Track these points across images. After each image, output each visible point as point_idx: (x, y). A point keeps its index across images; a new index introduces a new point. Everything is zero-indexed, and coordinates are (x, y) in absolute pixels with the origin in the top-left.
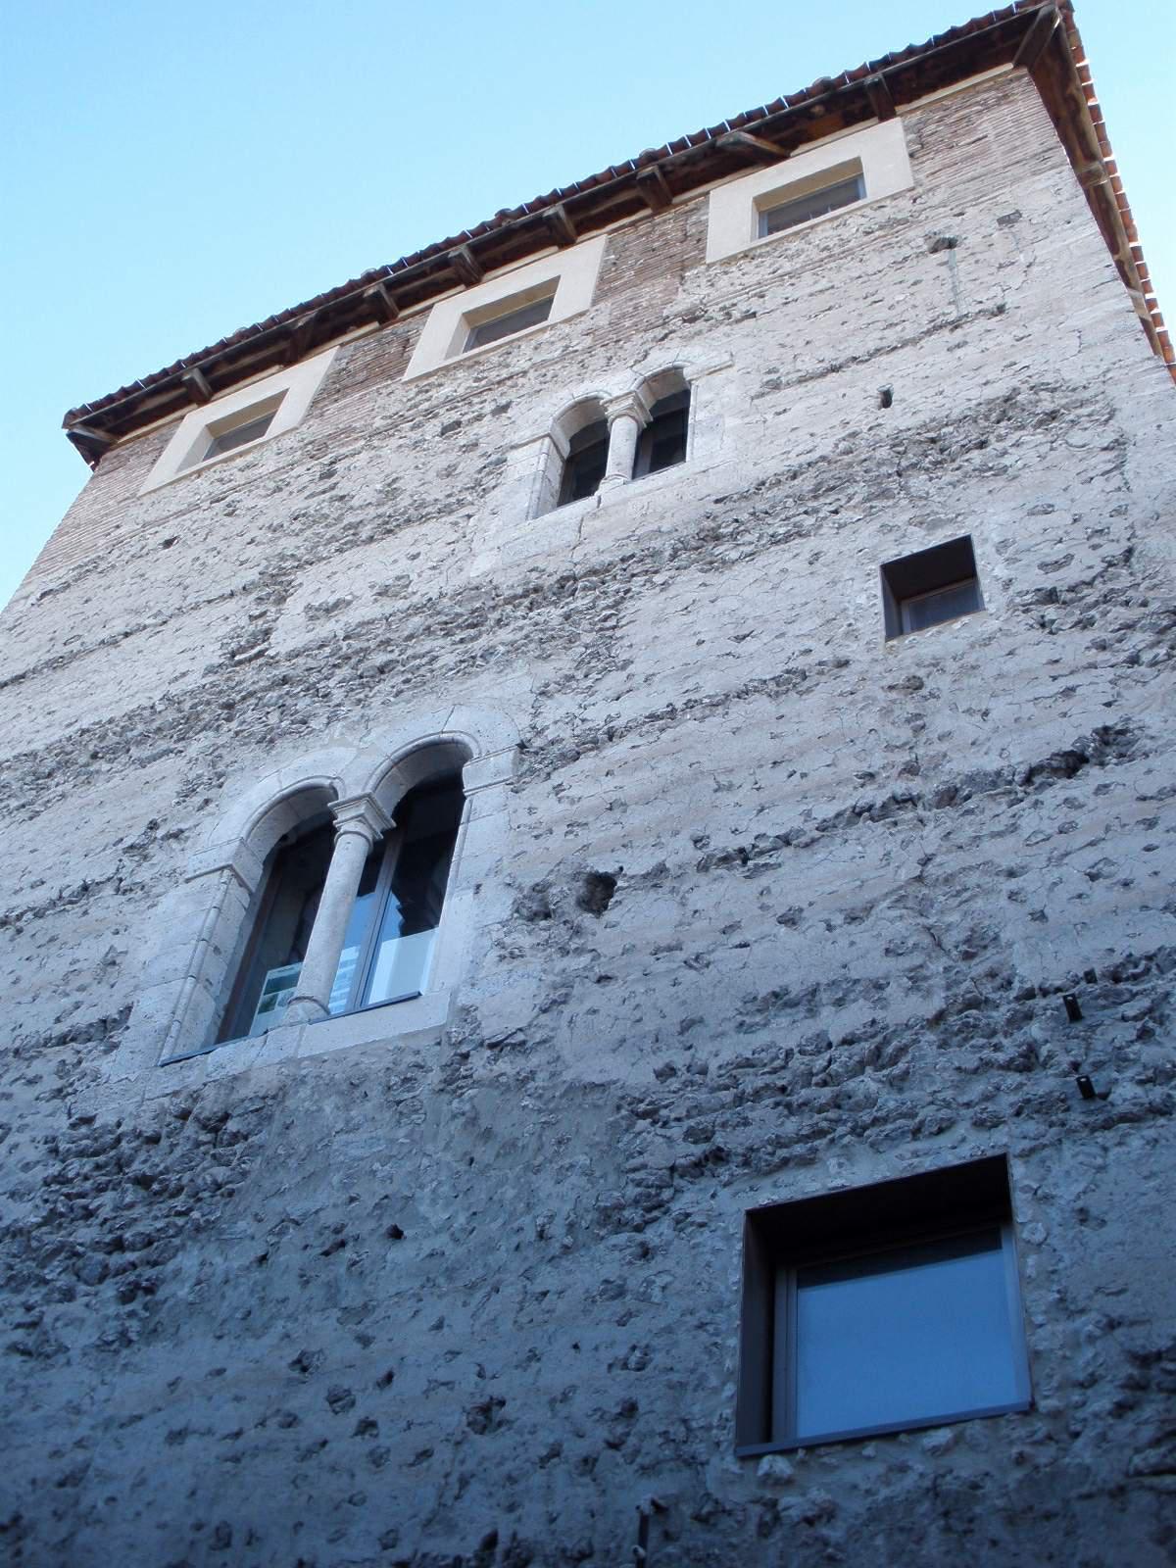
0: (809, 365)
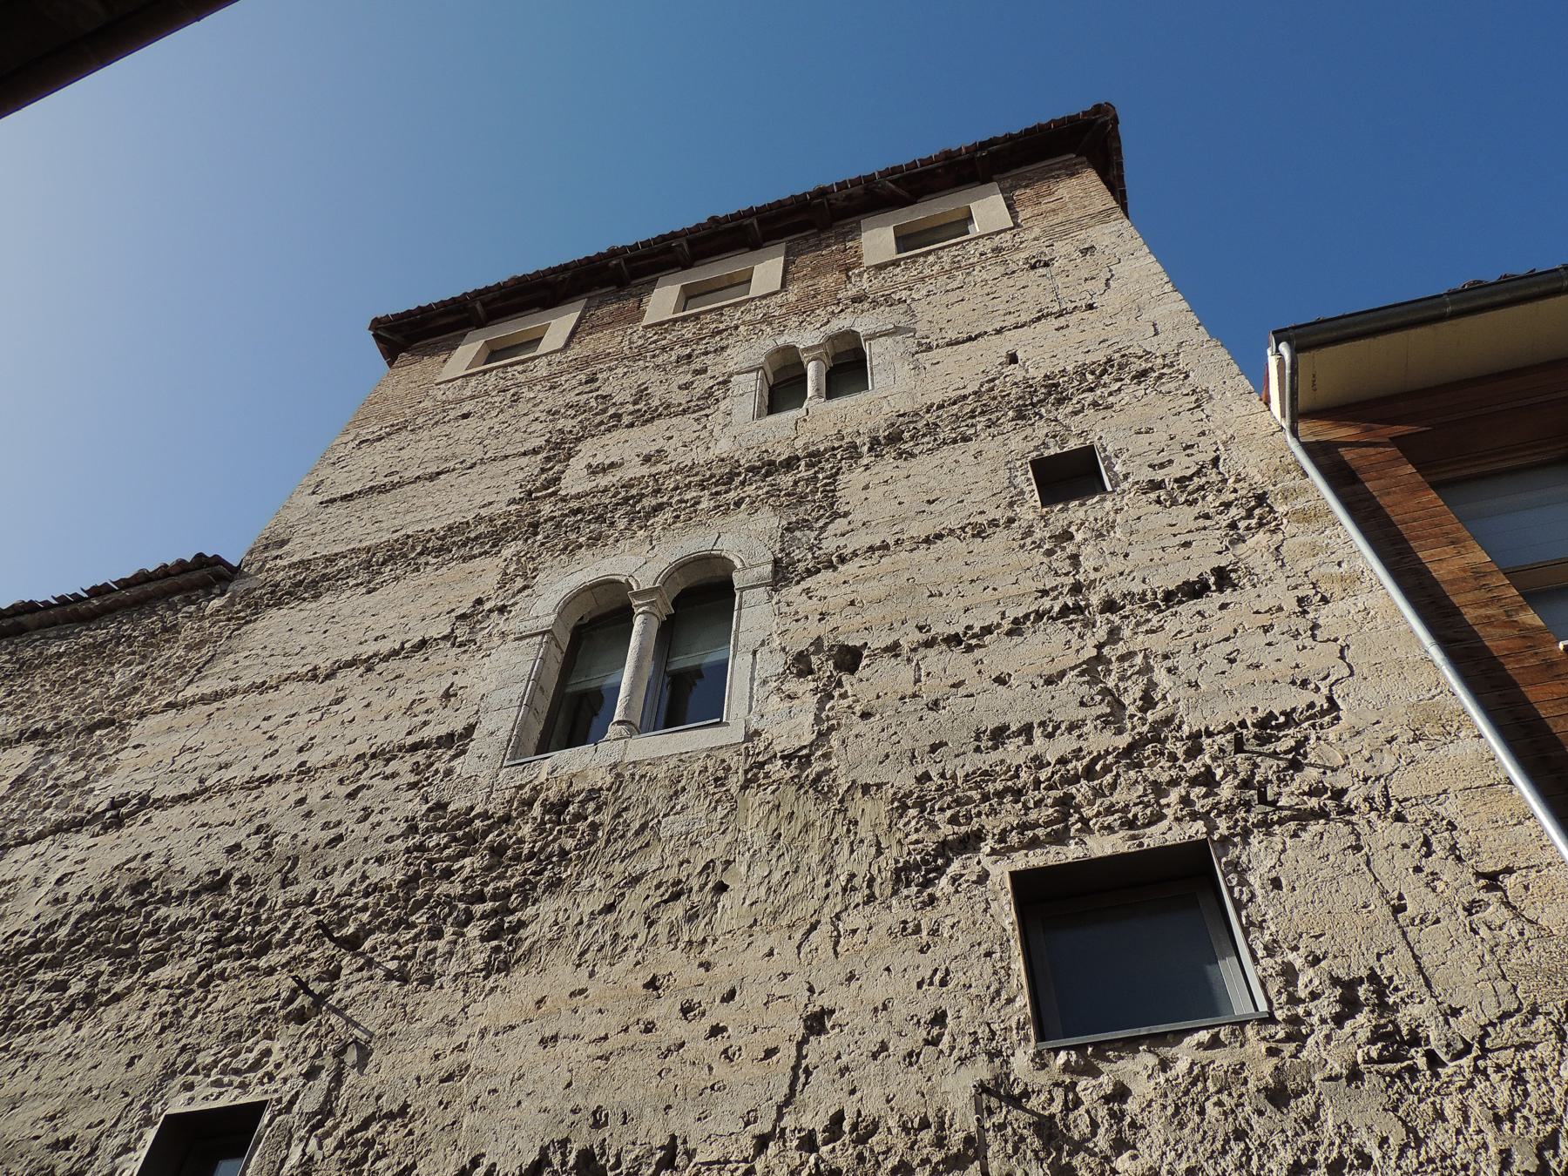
0: (952, 335)
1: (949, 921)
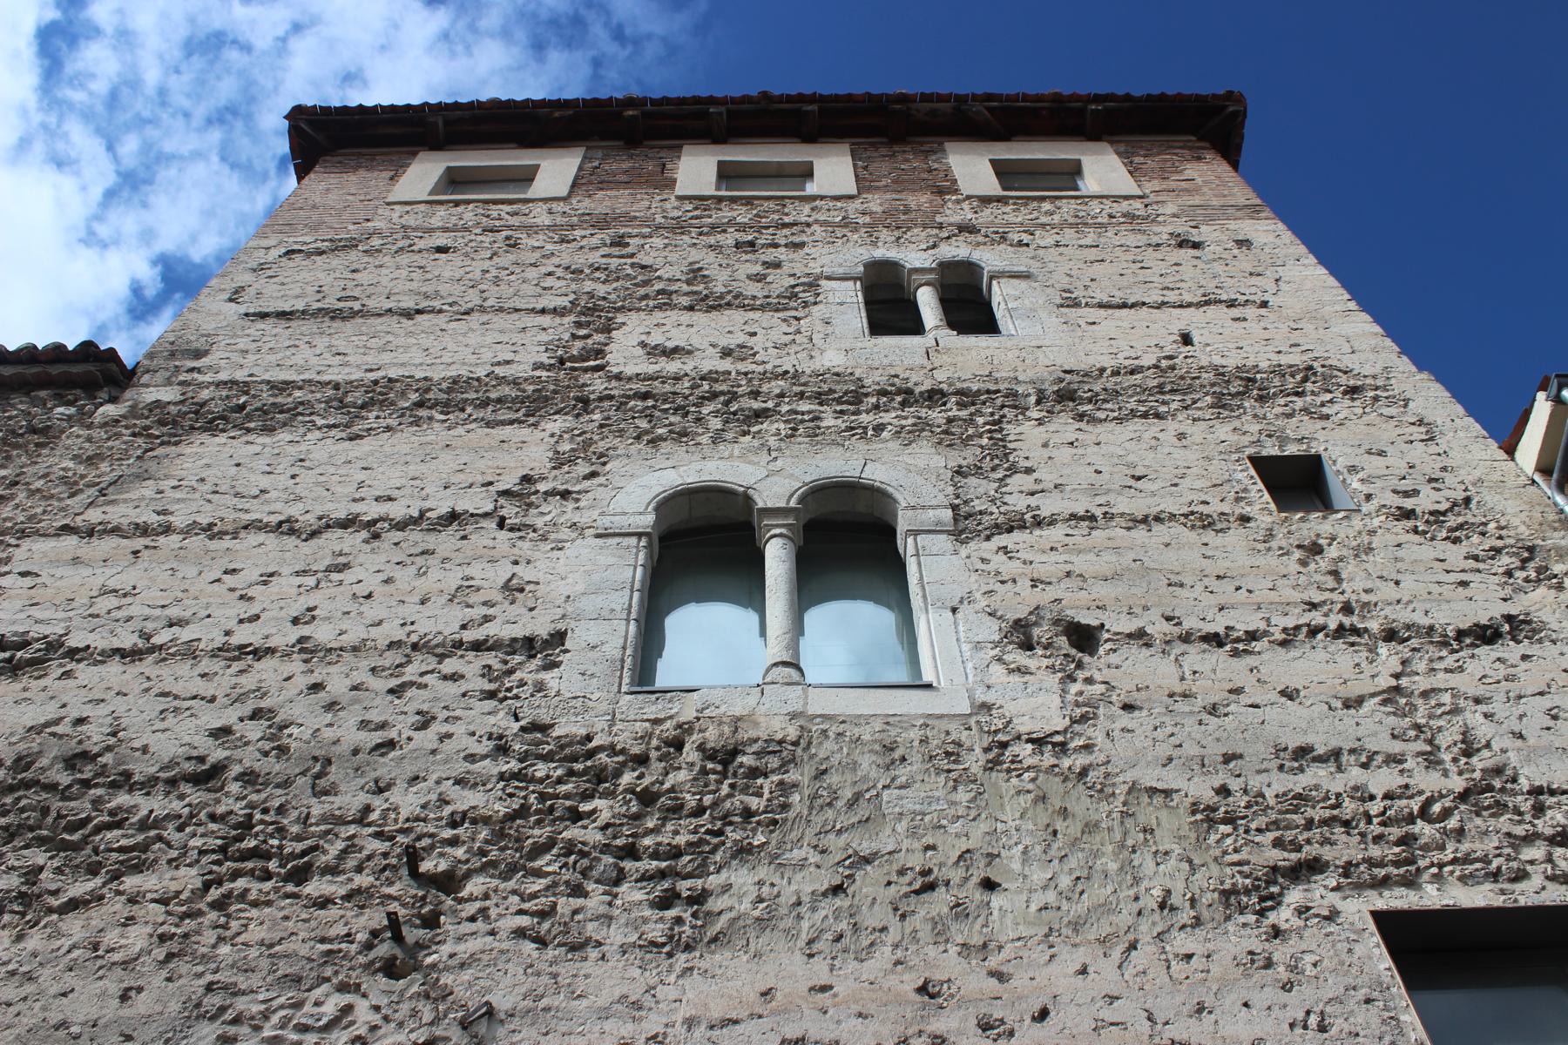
1: (1309, 958)
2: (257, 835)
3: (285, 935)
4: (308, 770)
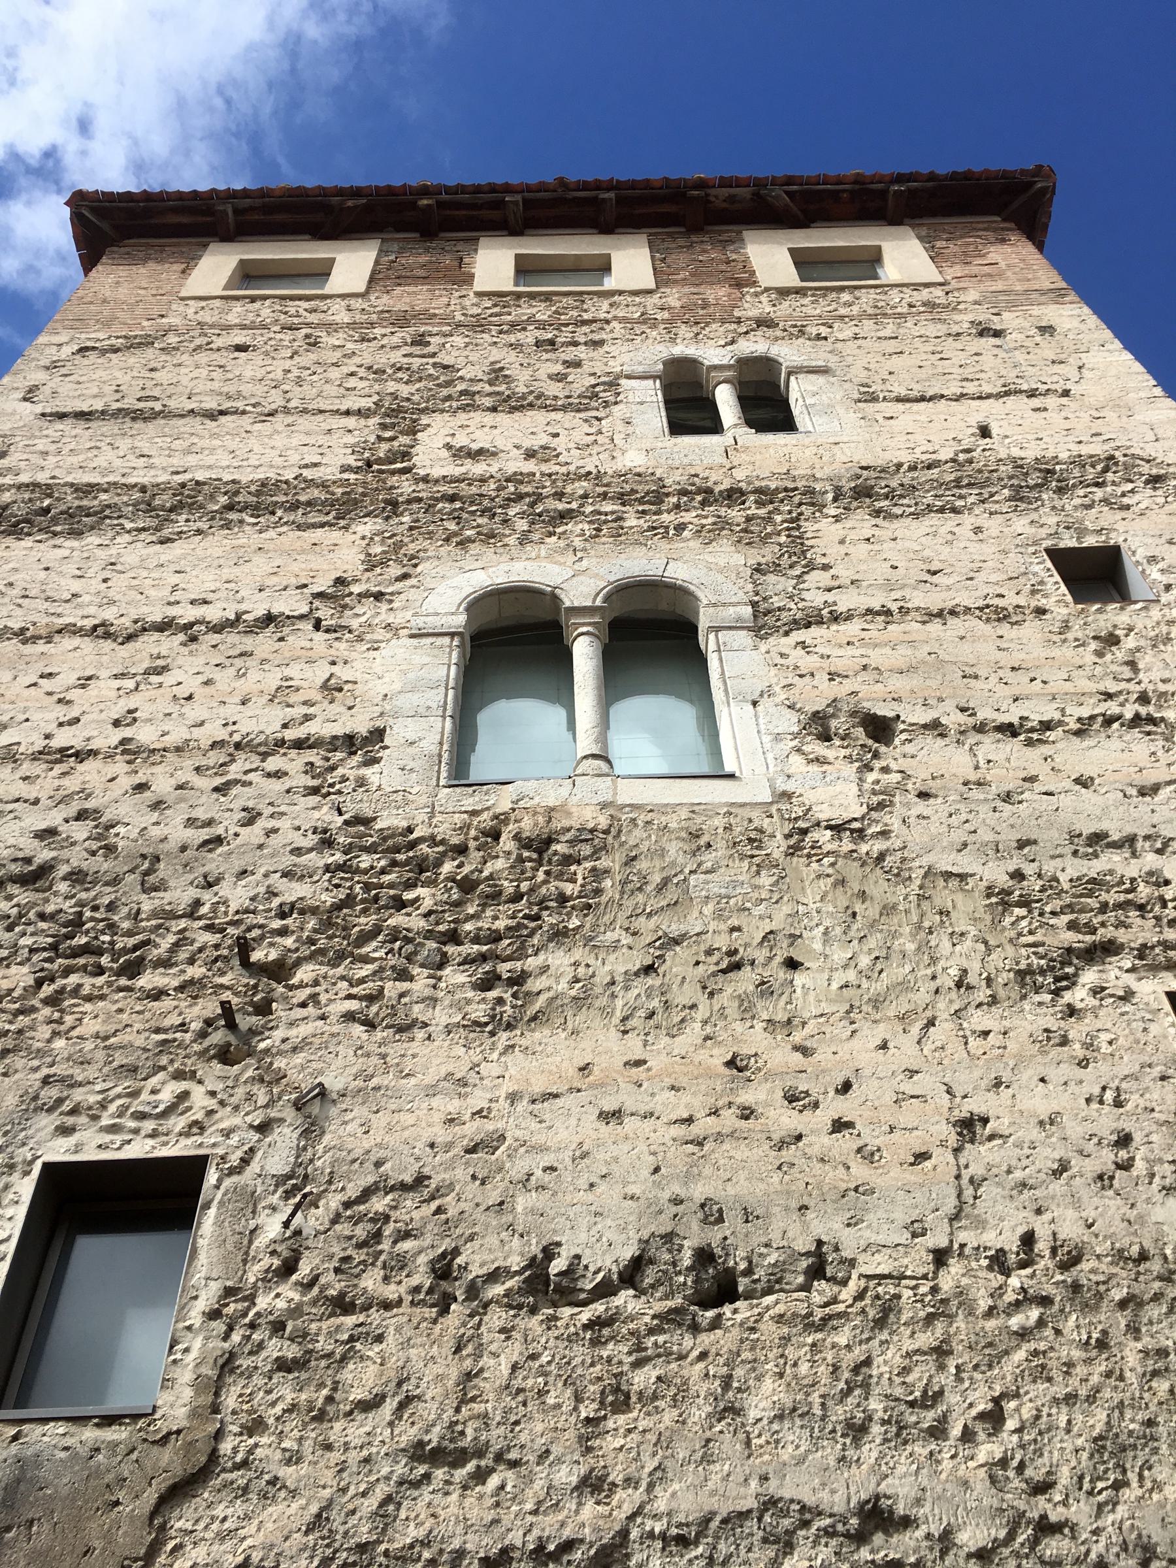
1: (1104, 1037)
2: (87, 932)
3: (120, 1027)
4: (136, 867)
